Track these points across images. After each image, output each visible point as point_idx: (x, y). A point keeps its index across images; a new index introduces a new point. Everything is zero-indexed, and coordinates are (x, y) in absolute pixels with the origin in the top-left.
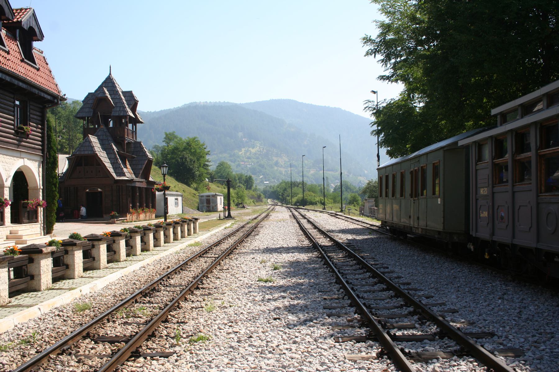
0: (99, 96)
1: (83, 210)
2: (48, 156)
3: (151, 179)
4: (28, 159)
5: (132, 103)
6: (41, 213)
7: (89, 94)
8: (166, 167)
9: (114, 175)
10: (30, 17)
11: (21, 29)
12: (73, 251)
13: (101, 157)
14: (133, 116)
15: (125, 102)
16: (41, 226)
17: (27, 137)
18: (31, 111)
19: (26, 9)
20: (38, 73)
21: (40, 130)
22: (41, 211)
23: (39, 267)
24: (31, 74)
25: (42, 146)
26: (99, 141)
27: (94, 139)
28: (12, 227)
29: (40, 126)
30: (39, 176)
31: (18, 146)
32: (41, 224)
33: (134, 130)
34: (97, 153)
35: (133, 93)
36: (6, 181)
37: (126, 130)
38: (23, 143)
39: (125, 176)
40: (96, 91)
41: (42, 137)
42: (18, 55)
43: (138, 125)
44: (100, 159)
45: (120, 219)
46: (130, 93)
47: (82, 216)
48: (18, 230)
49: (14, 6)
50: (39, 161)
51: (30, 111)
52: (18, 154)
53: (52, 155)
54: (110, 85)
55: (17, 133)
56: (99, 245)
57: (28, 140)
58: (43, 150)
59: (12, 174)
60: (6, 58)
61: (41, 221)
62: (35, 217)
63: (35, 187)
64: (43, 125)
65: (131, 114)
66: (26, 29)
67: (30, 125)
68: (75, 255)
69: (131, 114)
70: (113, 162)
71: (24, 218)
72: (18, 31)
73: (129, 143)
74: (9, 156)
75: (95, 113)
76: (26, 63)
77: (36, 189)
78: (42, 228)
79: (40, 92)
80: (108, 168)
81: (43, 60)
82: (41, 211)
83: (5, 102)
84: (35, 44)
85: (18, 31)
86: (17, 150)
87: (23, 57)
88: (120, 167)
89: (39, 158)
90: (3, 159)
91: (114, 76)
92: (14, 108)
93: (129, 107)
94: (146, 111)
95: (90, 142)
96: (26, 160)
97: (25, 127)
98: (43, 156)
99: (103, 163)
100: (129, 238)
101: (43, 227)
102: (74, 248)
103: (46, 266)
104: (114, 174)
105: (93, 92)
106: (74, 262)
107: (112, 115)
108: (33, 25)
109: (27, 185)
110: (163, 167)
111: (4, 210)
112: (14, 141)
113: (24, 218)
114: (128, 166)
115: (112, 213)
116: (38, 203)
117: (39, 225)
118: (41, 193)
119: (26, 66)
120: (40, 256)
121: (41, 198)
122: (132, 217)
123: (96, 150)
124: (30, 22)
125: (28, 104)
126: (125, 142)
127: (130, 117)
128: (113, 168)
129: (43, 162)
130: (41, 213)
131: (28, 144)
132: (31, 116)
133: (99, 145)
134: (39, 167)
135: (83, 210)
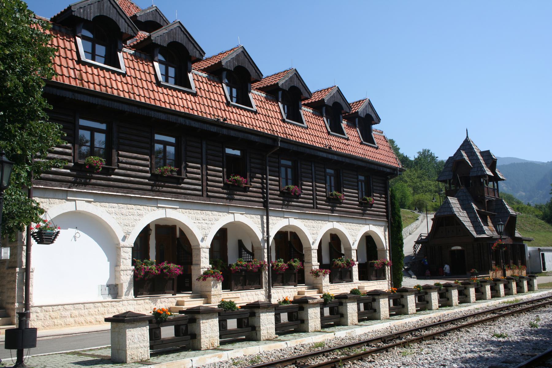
0: (457, 159)
1: (447, 268)
2: (392, 221)
3: (517, 235)
4: (373, 225)
5: (491, 161)
6: (388, 271)
7: (450, 158)
8: (502, 224)
9: (474, 234)
10: (366, 106)
11: (360, 117)
12: (346, 303)
13: (459, 217)
14: (492, 175)
15: (482, 161)
16: (389, 283)
17: (371, 206)
18: (374, 184)
19: (363, 100)
20: (378, 151)
21: (384, 199)
22: (388, 270)
23: (308, 314)
24: (369, 153)
25: (387, 212)
26: (459, 202)
27: (453, 201)
28: (360, 283)
29: (383, 196)
30: (385, 239)
31: (363, 214)
32: (388, 281)
33: (496, 187)
34: (455, 213)
35: (491, 152)
36: (353, 245)
37: (486, 189)
38: (368, 212)
39: (485, 233)
40: (454, 155)
41: (386, 205)
42: (357, 139)
43: (499, 182)
44: (459, 219)
45: (480, 276)
46: (488, 152)
47: (446, 273)
48: (364, 286)
49: (350, 100)
50: (384, 226)
51: (373, 183)
52: (364, 222)
53: (397, 219)
54: (468, 147)
55: (361, 204)
56: (379, 299)
57: (373, 209)
58: (387, 217)
59: (358, 238)
60: (345, 144)
61: (389, 278)
62: (382, 274)
63: (382, 249)
64: (386, 194)
65: (489, 173)
66: (363, 116)
67: (374, 196)
68: (348, 306)
69: (489, 173)
70: (473, 221)
71: (371, 276)
72: (357, 119)
73: (490, 202)
74: (355, 223)
75: (455, 176)
76: (364, 144)
77: (384, 251)
78: (390, 284)
79: (379, 167)
80: (468, 227)
81: (383, 138)
82: (388, 270)
83: (349, 179)
84: (374, 127)
85: (357, 119)
86: (361, 218)
87: (362, 140)
88: (480, 226)
89: (384, 224)
90: (349, 227)
91: (470, 138)
92: (358, 183)
93: (487, 166)
94: (546, 161)
95: (449, 203)
96: (371, 226)
97: (368, 198)
98: (388, 222)
99: (462, 223)
100: (424, 294)
101: (391, 283)
102: (347, 300)
103: (314, 314)
104: (475, 232)
105: (452, 155)
106: (347, 312)
107: (470, 175)
108: (370, 111)
109: (377, 248)
110: (499, 224)
111: (352, 269)
112: (358, 211)
113: (371, 276)
114: (490, 224)
115: (471, 270)
116: (383, 262)
117: (387, 282)
118: (388, 254)
119: (365, 147)
120: (308, 305)
121: (388, 258)
122: (496, 274)
123: (455, 210)
124: (366, 111)
125: (371, 179)
126: (485, 201)
127: (489, 176)
128: (473, 227)
129: (388, 227)
130: (388, 271)
131: (372, 212)
132: (374, 188)
133: (459, 206)
134: (385, 231)
135: (447, 268)
